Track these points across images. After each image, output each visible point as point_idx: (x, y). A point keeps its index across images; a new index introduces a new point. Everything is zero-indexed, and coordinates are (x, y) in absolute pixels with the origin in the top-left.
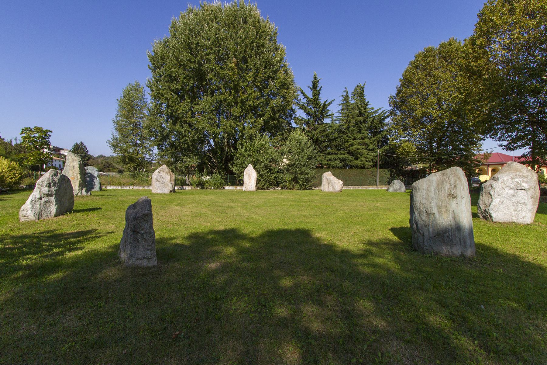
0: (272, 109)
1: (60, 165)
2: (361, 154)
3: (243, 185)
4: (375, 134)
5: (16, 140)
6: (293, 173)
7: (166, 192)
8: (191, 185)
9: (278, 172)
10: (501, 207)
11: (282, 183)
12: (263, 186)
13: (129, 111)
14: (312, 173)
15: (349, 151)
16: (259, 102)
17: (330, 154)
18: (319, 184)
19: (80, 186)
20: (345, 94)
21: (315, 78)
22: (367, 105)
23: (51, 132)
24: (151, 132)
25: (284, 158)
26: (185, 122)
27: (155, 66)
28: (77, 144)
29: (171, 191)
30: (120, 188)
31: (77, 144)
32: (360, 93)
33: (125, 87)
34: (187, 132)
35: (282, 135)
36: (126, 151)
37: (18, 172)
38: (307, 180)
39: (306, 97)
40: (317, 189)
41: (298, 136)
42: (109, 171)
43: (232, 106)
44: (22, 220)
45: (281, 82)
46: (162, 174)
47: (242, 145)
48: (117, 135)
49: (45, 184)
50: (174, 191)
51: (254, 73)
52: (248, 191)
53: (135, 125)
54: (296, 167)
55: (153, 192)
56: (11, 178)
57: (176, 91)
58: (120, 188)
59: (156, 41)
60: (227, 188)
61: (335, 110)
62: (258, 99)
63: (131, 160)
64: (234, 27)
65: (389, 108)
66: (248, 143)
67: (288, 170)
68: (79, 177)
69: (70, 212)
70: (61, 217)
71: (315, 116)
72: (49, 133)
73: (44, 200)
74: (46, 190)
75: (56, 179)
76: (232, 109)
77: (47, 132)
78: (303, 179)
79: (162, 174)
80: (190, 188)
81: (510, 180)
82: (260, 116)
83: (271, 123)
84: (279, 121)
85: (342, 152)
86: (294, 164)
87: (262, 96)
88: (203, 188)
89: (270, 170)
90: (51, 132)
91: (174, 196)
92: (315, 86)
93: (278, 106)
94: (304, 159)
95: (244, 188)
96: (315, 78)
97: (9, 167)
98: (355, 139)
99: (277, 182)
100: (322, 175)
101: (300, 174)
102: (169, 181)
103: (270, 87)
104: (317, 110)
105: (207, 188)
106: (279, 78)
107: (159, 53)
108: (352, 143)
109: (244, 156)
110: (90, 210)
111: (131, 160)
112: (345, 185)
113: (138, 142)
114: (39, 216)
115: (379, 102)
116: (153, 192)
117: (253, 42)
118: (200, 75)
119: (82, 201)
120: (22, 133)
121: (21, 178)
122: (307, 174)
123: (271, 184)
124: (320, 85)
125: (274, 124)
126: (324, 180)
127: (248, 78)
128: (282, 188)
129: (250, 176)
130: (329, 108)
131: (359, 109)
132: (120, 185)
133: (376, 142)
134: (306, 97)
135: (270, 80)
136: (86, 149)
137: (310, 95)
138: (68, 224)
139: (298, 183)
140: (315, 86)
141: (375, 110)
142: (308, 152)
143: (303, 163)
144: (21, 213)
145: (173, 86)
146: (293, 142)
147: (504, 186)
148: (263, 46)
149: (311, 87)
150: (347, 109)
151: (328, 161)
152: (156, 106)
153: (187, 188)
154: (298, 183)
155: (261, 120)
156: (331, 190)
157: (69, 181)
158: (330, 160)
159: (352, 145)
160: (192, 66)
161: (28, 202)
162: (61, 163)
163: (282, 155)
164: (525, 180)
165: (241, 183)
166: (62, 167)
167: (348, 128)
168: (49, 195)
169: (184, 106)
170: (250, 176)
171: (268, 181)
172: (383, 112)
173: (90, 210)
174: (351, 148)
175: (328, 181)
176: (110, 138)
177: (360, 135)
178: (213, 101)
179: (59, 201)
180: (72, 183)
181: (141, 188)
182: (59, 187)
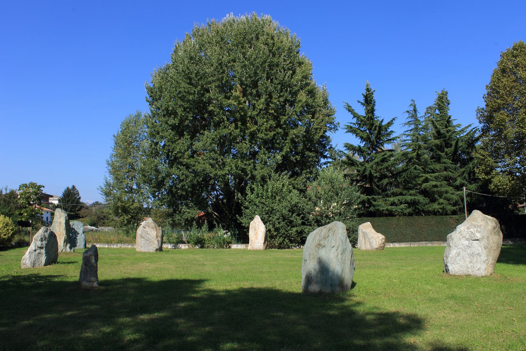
0: (293, 141)
1: (47, 218)
2: (441, 195)
3: (248, 243)
4: (464, 163)
5: (6, 189)
7: (151, 251)
8: (188, 242)
12: (280, 244)
13: (126, 148)
16: (272, 134)
17: (394, 194)
19: (64, 242)
20: (412, 109)
23: (44, 187)
24: (145, 176)
26: (181, 164)
27: (153, 99)
28: (68, 188)
29: (157, 250)
30: (107, 246)
31: (68, 188)
32: (442, 102)
34: (184, 176)
36: (119, 199)
37: (11, 228)
39: (355, 115)
42: (104, 224)
44: (23, 267)
46: (147, 229)
47: (252, 190)
48: (111, 179)
49: (39, 238)
50: (160, 249)
51: (266, 100)
52: (254, 251)
53: (131, 165)
55: (137, 250)
56: (5, 235)
57: (174, 127)
58: (107, 246)
59: (149, 77)
60: (234, 246)
61: (400, 131)
63: (125, 210)
65: (481, 126)
68: (65, 233)
69: (55, 263)
70: (48, 266)
71: (367, 139)
73: (38, 251)
74: (39, 243)
75: (47, 235)
77: (40, 186)
79: (147, 229)
80: (187, 247)
81: (466, 230)
83: (293, 159)
84: (303, 156)
85: (411, 192)
87: (279, 125)
88: (202, 247)
90: (44, 187)
91: (160, 254)
92: (368, 101)
95: (250, 247)
96: (368, 90)
97: (4, 223)
102: (155, 238)
103: (288, 114)
104: (372, 131)
105: (208, 247)
107: (157, 85)
110: (69, 263)
111: (125, 210)
112: (388, 240)
113: (135, 187)
114: (34, 264)
115: (466, 117)
116: (137, 250)
118: (200, 107)
119: (65, 256)
121: (13, 235)
124: (376, 97)
125: (296, 159)
129: (257, 230)
130: (390, 129)
131: (436, 128)
132: (108, 242)
134: (355, 115)
135: (287, 106)
136: (78, 195)
137: (361, 111)
138: (52, 270)
141: (462, 127)
144: (23, 262)
145: (172, 121)
147: (461, 237)
149: (363, 102)
150: (416, 129)
152: (151, 146)
153: (183, 247)
156: (368, 247)
157: (55, 236)
159: (426, 180)
160: (191, 97)
161: (27, 253)
162: (49, 215)
164: (479, 229)
166: (49, 220)
168: (41, 248)
169: (182, 143)
170: (257, 230)
171: (289, 237)
172: (472, 130)
173: (69, 263)
175: (365, 234)
176: (102, 184)
177: (438, 166)
178: (216, 136)
179: (47, 253)
180: (58, 239)
181: (130, 247)
182: (48, 242)
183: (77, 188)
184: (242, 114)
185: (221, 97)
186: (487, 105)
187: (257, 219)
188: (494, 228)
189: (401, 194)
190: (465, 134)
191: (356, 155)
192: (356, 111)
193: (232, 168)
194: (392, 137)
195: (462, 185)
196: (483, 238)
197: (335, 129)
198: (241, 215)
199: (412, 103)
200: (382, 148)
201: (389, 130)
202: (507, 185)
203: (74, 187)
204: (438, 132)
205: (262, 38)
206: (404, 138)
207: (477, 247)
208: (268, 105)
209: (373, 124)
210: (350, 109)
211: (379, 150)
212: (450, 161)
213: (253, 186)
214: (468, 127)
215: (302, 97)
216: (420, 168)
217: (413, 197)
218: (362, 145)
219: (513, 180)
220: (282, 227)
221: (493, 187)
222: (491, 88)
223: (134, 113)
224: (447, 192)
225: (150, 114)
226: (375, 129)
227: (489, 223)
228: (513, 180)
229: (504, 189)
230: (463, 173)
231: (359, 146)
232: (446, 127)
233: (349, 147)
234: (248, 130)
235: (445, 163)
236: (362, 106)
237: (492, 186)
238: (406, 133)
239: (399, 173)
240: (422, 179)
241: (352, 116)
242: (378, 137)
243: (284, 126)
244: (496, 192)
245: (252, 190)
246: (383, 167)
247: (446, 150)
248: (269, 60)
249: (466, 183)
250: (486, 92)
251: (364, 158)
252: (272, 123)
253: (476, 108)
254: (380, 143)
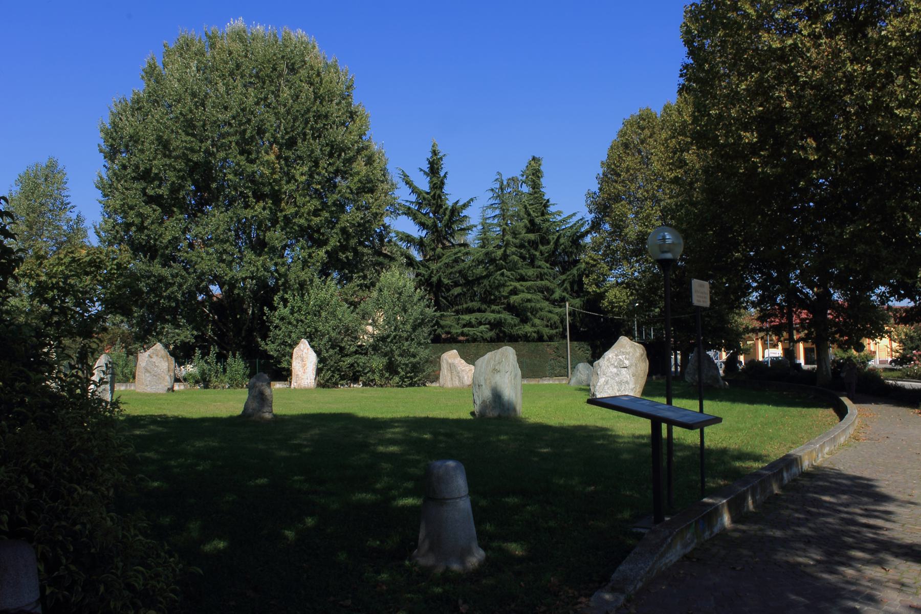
0: (344, 230)
2: (534, 311)
4: (565, 268)
6: (385, 355)
7: (161, 392)
8: (185, 380)
9: (356, 352)
10: (606, 387)
11: (366, 374)
12: (327, 381)
14: (424, 353)
15: (509, 304)
17: (470, 311)
18: (436, 379)
20: (498, 186)
21: (435, 153)
22: (546, 206)
25: (368, 324)
29: (169, 389)
32: (534, 175)
33: (22, 170)
35: (365, 277)
38: (415, 368)
39: (414, 190)
40: (434, 385)
41: (398, 278)
43: (268, 229)
45: (360, 181)
46: (155, 359)
50: (171, 389)
54: (391, 342)
62: (316, 213)
64: (272, 82)
65: (590, 217)
66: (298, 298)
67: (375, 348)
71: (433, 229)
76: (268, 234)
78: (406, 365)
79: (155, 359)
80: (182, 387)
82: (320, 244)
83: (342, 256)
85: (493, 307)
86: (388, 336)
88: (206, 387)
89: (342, 349)
91: (172, 396)
92: (434, 168)
93: (354, 225)
94: (408, 327)
96: (435, 153)
98: (522, 279)
99: (354, 374)
100: (439, 358)
101: (401, 355)
104: (439, 216)
106: (358, 173)
108: (515, 288)
109: (290, 323)
115: (570, 200)
117: (308, 111)
122: (414, 356)
123: (342, 378)
124: (446, 167)
125: (347, 257)
126: (444, 366)
127: (297, 177)
128: (365, 384)
130: (464, 213)
131: (529, 215)
133: (567, 285)
134: (414, 190)
137: (424, 184)
139: (397, 373)
140: (434, 168)
141: (563, 216)
142: (415, 312)
143: (405, 335)
146: (385, 292)
148: (326, 117)
149: (427, 170)
151: (464, 326)
154: (397, 373)
155: (321, 253)
156: (457, 383)
158: (469, 324)
159: (515, 292)
163: (363, 318)
165: (284, 375)
167: (505, 256)
172: (578, 222)
174: (514, 299)
175: (452, 367)
177: (531, 272)
184: (277, 188)
185: (242, 159)
186: (600, 189)
188: (642, 355)
189: (479, 310)
192: (415, 184)
193: (258, 269)
195: (563, 300)
196: (631, 365)
198: (264, 337)
201: (462, 215)
202: (624, 301)
204: (532, 222)
205: (303, 73)
207: (626, 375)
208: (311, 176)
209: (441, 206)
211: (447, 244)
212: (548, 265)
213: (286, 296)
215: (360, 166)
216: (509, 273)
217: (498, 316)
219: (632, 294)
220: (331, 356)
221: (606, 304)
222: (609, 166)
223: (44, 162)
224: (541, 309)
226: (445, 214)
228: (632, 294)
229: (620, 307)
230: (564, 281)
232: (543, 214)
233: (408, 239)
234: (281, 211)
235: (539, 267)
237: (605, 303)
239: (478, 280)
240: (508, 289)
242: (449, 225)
243: (334, 209)
244: (608, 312)
245: (285, 301)
246: (453, 270)
247: (541, 247)
248: (315, 108)
249: (567, 296)
250: (601, 171)
251: (425, 256)
252: (316, 203)
253: (586, 192)
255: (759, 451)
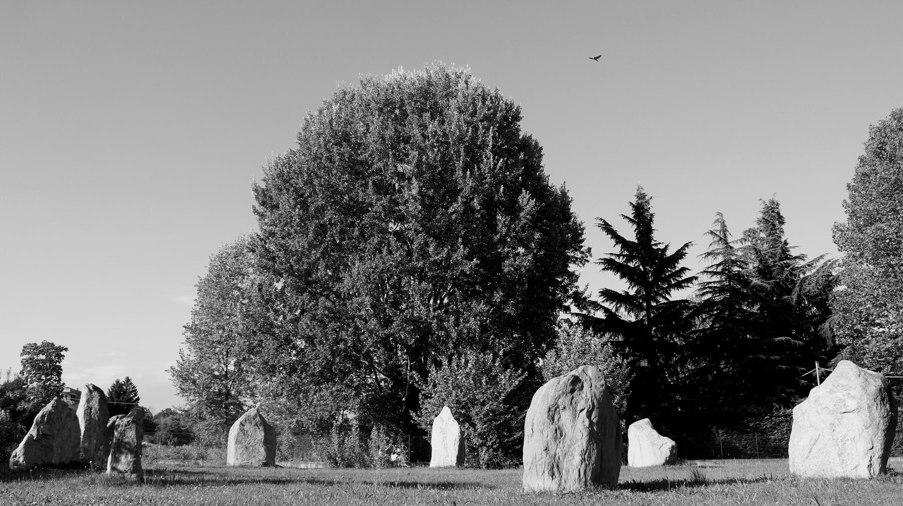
5: (8, 373)
28: (118, 382)
31: (118, 382)
32: (773, 219)
39: (619, 239)
59: (257, 171)
72: (63, 353)
90: (66, 350)
92: (642, 217)
104: (646, 261)
120: (22, 355)
124: (654, 208)
134: (619, 239)
137: (630, 233)
141: (807, 261)
149: (632, 217)
172: (825, 264)
176: (173, 361)
183: (134, 381)
187: (446, 413)
190: (814, 271)
191: (622, 309)
194: (685, 276)
197: (583, 261)
198: (615, 344)
199: (718, 217)
200: (667, 296)
203: (128, 380)
206: (705, 278)
210: (608, 228)
214: (818, 260)
218: (632, 292)
225: (260, 233)
227: (871, 380)
231: (627, 293)
233: (609, 295)
236: (631, 224)
238: (710, 270)
241: (613, 242)
254: (663, 289)
255: (827, 381)
